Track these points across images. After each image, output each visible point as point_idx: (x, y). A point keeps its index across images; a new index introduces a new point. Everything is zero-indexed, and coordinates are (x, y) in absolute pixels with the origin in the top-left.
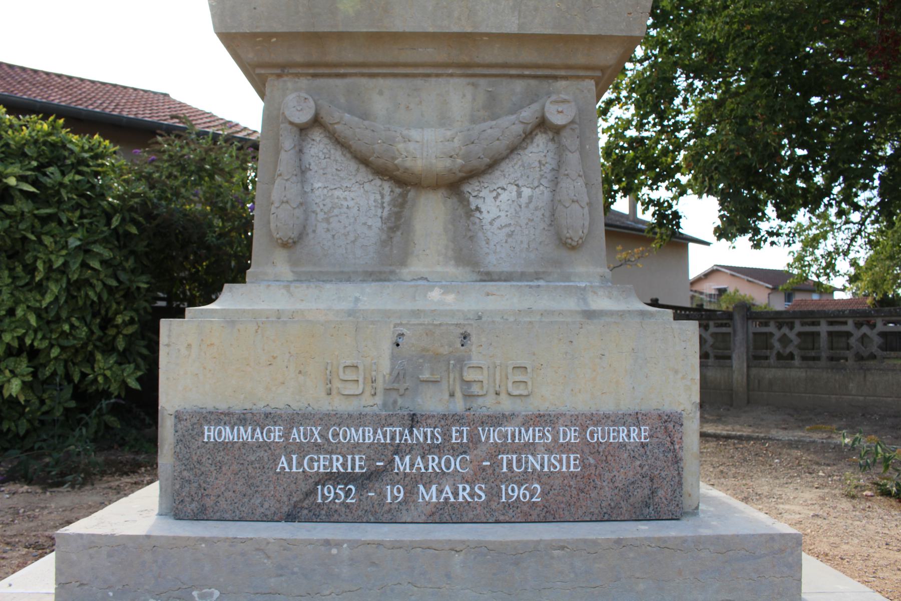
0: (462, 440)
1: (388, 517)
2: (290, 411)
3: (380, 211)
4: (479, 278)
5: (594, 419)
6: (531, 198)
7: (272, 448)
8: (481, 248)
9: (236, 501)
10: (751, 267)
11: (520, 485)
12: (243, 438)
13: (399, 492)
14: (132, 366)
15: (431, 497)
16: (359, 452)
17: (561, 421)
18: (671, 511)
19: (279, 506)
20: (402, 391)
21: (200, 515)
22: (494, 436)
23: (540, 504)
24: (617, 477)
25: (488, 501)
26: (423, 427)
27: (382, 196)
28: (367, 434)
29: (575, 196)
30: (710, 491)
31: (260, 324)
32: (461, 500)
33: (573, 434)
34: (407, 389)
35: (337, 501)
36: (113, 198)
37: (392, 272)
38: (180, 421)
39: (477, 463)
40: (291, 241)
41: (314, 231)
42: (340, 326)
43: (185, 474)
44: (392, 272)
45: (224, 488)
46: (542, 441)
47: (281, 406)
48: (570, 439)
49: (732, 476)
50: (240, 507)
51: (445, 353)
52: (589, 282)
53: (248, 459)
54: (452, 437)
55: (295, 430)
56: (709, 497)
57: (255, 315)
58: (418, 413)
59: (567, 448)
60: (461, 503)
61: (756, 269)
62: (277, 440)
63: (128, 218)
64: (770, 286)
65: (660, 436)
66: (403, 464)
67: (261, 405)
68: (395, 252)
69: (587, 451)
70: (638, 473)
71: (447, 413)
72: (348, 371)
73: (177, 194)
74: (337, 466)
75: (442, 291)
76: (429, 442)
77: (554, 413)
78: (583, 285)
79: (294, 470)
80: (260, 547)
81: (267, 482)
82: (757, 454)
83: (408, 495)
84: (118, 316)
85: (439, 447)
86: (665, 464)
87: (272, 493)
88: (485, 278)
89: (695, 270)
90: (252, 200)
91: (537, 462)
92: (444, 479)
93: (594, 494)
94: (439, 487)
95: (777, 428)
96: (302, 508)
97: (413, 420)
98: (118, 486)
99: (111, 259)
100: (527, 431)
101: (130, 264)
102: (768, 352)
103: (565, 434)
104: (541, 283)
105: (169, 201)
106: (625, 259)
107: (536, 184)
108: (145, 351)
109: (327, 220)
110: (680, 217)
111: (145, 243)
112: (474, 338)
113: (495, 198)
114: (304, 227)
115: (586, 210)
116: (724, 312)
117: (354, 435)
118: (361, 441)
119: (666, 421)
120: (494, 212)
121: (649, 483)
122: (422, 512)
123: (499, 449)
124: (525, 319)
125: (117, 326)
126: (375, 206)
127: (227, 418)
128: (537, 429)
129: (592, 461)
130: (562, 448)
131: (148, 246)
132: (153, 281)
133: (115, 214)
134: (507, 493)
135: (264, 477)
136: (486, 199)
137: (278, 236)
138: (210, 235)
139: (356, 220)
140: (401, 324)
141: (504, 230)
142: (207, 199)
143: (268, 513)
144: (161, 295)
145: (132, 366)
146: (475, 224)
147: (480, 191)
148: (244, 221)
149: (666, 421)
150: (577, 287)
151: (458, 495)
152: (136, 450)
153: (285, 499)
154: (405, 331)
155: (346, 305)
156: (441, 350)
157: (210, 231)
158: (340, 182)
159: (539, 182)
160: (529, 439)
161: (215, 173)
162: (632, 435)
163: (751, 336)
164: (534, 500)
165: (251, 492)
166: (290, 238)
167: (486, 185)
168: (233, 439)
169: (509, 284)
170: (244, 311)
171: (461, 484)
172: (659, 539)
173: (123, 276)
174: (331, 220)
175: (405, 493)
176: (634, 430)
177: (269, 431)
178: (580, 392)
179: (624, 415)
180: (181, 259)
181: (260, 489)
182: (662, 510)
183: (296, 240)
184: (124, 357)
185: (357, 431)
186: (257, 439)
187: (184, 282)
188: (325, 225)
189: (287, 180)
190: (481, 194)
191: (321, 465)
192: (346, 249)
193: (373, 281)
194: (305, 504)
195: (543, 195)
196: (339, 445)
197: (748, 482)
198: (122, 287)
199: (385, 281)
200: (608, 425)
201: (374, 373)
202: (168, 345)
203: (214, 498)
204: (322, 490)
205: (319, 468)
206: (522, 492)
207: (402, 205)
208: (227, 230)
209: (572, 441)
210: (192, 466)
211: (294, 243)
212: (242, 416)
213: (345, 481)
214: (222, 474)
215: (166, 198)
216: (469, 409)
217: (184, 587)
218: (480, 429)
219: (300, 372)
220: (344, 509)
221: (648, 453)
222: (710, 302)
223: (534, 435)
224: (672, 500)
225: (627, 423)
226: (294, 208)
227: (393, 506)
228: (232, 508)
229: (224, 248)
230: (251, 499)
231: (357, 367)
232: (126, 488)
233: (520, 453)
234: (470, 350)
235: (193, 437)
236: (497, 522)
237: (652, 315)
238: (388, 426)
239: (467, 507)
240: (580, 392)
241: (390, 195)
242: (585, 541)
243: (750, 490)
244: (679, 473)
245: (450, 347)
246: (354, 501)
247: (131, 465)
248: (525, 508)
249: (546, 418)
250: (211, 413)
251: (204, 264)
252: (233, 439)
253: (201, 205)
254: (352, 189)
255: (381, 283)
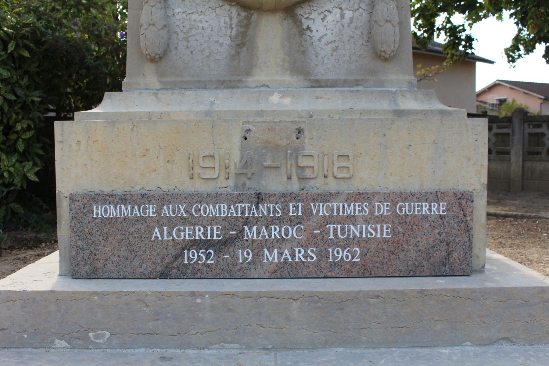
0: (297, 214)
1: (240, 274)
2: (162, 193)
3: (229, 31)
4: (309, 85)
5: (402, 196)
6: (352, 19)
7: (148, 221)
8: (312, 61)
9: (120, 263)
10: (527, 81)
11: (343, 248)
12: (124, 214)
13: (248, 254)
14: (31, 163)
15: (274, 258)
16: (217, 224)
17: (376, 198)
18: (462, 269)
19: (154, 267)
20: (249, 175)
21: (92, 275)
22: (323, 210)
23: (360, 263)
24: (420, 243)
25: (319, 261)
26: (267, 203)
27: (231, 19)
28: (222, 210)
29: (388, 16)
30: (493, 255)
31: (135, 124)
32: (297, 260)
33: (386, 208)
34: (254, 173)
35: (199, 262)
36: (8, 27)
37: (240, 81)
38: (74, 202)
39: (310, 231)
40: (157, 57)
41: (176, 48)
42: (200, 124)
43: (80, 243)
44: (240, 81)
45: (111, 254)
46: (361, 214)
47: (154, 188)
48: (384, 212)
49: (508, 246)
50: (123, 268)
51: (284, 145)
52: (399, 87)
53: (129, 231)
54: (289, 211)
55: (165, 207)
56: (493, 259)
57: (130, 117)
58: (263, 192)
59: (381, 219)
60: (297, 262)
61: (531, 83)
62: (151, 215)
63: (21, 45)
64: (542, 97)
65: (455, 210)
66: (251, 233)
67: (138, 188)
68: (242, 64)
69: (396, 222)
70: (437, 239)
71: (285, 192)
72: (207, 160)
73: (60, 24)
74: (199, 235)
75: (281, 95)
76: (271, 215)
77: (370, 191)
78: (394, 89)
79: (165, 238)
80: (141, 298)
81: (144, 248)
82: (529, 229)
83: (255, 257)
84: (17, 124)
85: (280, 219)
86: (459, 232)
87: (149, 256)
88: (315, 84)
89: (480, 85)
90: (124, 28)
91: (357, 231)
92: (284, 244)
93: (402, 256)
94: (279, 251)
95: (546, 209)
96: (172, 268)
97: (258, 198)
98: (25, 257)
99: (9, 78)
100: (349, 206)
101: (25, 82)
102: (540, 149)
103: (379, 208)
104: (360, 88)
105: (54, 30)
106: (424, 75)
107: (356, 7)
108: (41, 152)
109: (186, 39)
110: (473, 40)
111: (36, 65)
112: (306, 133)
113: (323, 19)
114: (168, 45)
115: (397, 28)
116: (505, 117)
117: (213, 210)
118: (218, 215)
119: (460, 198)
120: (322, 31)
121: (445, 247)
122: (267, 270)
123: (327, 220)
124: (348, 117)
125: (17, 132)
126: (225, 27)
127: (111, 199)
128: (357, 204)
129: (401, 230)
130: (377, 219)
131: (38, 67)
132: (45, 95)
133: (10, 41)
134: (333, 255)
135: (142, 245)
136: (316, 20)
137: (147, 52)
138: (89, 57)
139: (210, 39)
140: (248, 122)
141: (330, 45)
142: (84, 28)
143: (146, 272)
144: (51, 107)
145: (31, 163)
146: (306, 41)
147: (311, 14)
148: (116, 46)
149: (460, 198)
150: (390, 92)
151: (295, 256)
152: (37, 230)
153: (159, 261)
154: (251, 127)
155: (202, 108)
156: (280, 142)
157: (89, 55)
158: (196, 7)
159: (359, 5)
160: (351, 213)
161: (90, 6)
162: (433, 209)
163: (526, 135)
164: (354, 260)
165: (132, 256)
166: (157, 54)
167: (315, 8)
168: (117, 215)
169: (334, 89)
170: (122, 113)
171: (297, 247)
172: (454, 290)
173: (20, 92)
174: (190, 39)
175: (253, 256)
176: (434, 205)
177: (145, 208)
178: (391, 175)
179: (426, 193)
180: (66, 78)
181: (139, 254)
182: (455, 268)
183: (161, 55)
184: (24, 157)
185: (214, 207)
186: (136, 214)
187: (70, 96)
188: (185, 43)
189: (153, 6)
190: (311, 16)
191: (186, 234)
192: (202, 62)
193: (224, 88)
194: (175, 264)
195: (362, 16)
196: (200, 219)
197: (522, 250)
198: (19, 101)
199: (234, 88)
200: (414, 202)
201: (227, 161)
202: (62, 142)
203: (103, 261)
204: (188, 254)
205: (185, 236)
206: (345, 254)
207: (247, 26)
208: (102, 53)
209: (385, 214)
210: (85, 237)
211: (160, 58)
212: (123, 197)
213: (206, 247)
214: (108, 243)
215: (52, 28)
216: (303, 189)
217: (83, 330)
218: (312, 204)
219: (168, 161)
220: (205, 269)
221: (445, 223)
222: (492, 110)
223: (355, 209)
224: (463, 260)
225: (429, 200)
226: (159, 30)
227: (244, 266)
228: (117, 269)
229: (100, 68)
230: (132, 262)
231: (213, 156)
232: (31, 259)
233: (343, 224)
234: (304, 142)
235: (84, 214)
236: (326, 277)
237: (450, 113)
238: (239, 203)
239: (302, 266)
240: (391, 175)
241: (237, 18)
242: (395, 292)
243: (523, 257)
244: (470, 240)
245: (288, 139)
246: (213, 262)
247: (34, 242)
248: (348, 266)
249: (364, 196)
250: (98, 195)
251: (85, 81)
252: (117, 215)
253: (80, 33)
254: (206, 13)
255: (230, 90)
